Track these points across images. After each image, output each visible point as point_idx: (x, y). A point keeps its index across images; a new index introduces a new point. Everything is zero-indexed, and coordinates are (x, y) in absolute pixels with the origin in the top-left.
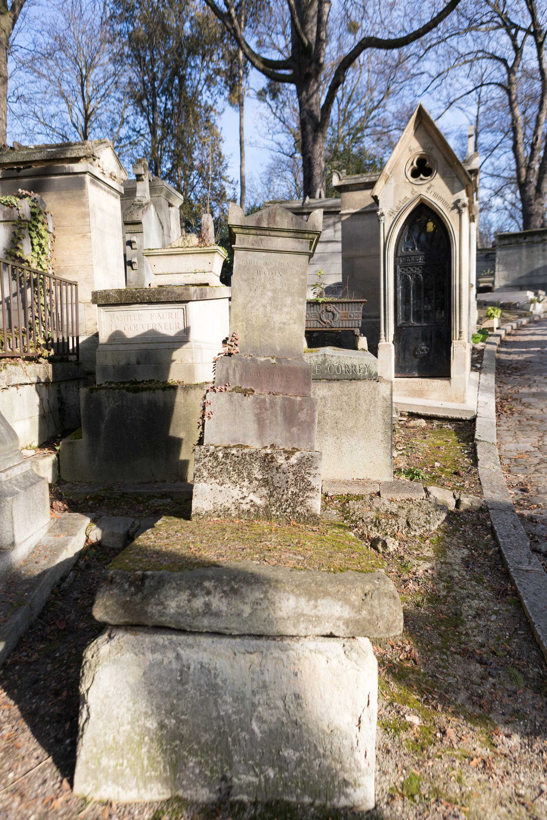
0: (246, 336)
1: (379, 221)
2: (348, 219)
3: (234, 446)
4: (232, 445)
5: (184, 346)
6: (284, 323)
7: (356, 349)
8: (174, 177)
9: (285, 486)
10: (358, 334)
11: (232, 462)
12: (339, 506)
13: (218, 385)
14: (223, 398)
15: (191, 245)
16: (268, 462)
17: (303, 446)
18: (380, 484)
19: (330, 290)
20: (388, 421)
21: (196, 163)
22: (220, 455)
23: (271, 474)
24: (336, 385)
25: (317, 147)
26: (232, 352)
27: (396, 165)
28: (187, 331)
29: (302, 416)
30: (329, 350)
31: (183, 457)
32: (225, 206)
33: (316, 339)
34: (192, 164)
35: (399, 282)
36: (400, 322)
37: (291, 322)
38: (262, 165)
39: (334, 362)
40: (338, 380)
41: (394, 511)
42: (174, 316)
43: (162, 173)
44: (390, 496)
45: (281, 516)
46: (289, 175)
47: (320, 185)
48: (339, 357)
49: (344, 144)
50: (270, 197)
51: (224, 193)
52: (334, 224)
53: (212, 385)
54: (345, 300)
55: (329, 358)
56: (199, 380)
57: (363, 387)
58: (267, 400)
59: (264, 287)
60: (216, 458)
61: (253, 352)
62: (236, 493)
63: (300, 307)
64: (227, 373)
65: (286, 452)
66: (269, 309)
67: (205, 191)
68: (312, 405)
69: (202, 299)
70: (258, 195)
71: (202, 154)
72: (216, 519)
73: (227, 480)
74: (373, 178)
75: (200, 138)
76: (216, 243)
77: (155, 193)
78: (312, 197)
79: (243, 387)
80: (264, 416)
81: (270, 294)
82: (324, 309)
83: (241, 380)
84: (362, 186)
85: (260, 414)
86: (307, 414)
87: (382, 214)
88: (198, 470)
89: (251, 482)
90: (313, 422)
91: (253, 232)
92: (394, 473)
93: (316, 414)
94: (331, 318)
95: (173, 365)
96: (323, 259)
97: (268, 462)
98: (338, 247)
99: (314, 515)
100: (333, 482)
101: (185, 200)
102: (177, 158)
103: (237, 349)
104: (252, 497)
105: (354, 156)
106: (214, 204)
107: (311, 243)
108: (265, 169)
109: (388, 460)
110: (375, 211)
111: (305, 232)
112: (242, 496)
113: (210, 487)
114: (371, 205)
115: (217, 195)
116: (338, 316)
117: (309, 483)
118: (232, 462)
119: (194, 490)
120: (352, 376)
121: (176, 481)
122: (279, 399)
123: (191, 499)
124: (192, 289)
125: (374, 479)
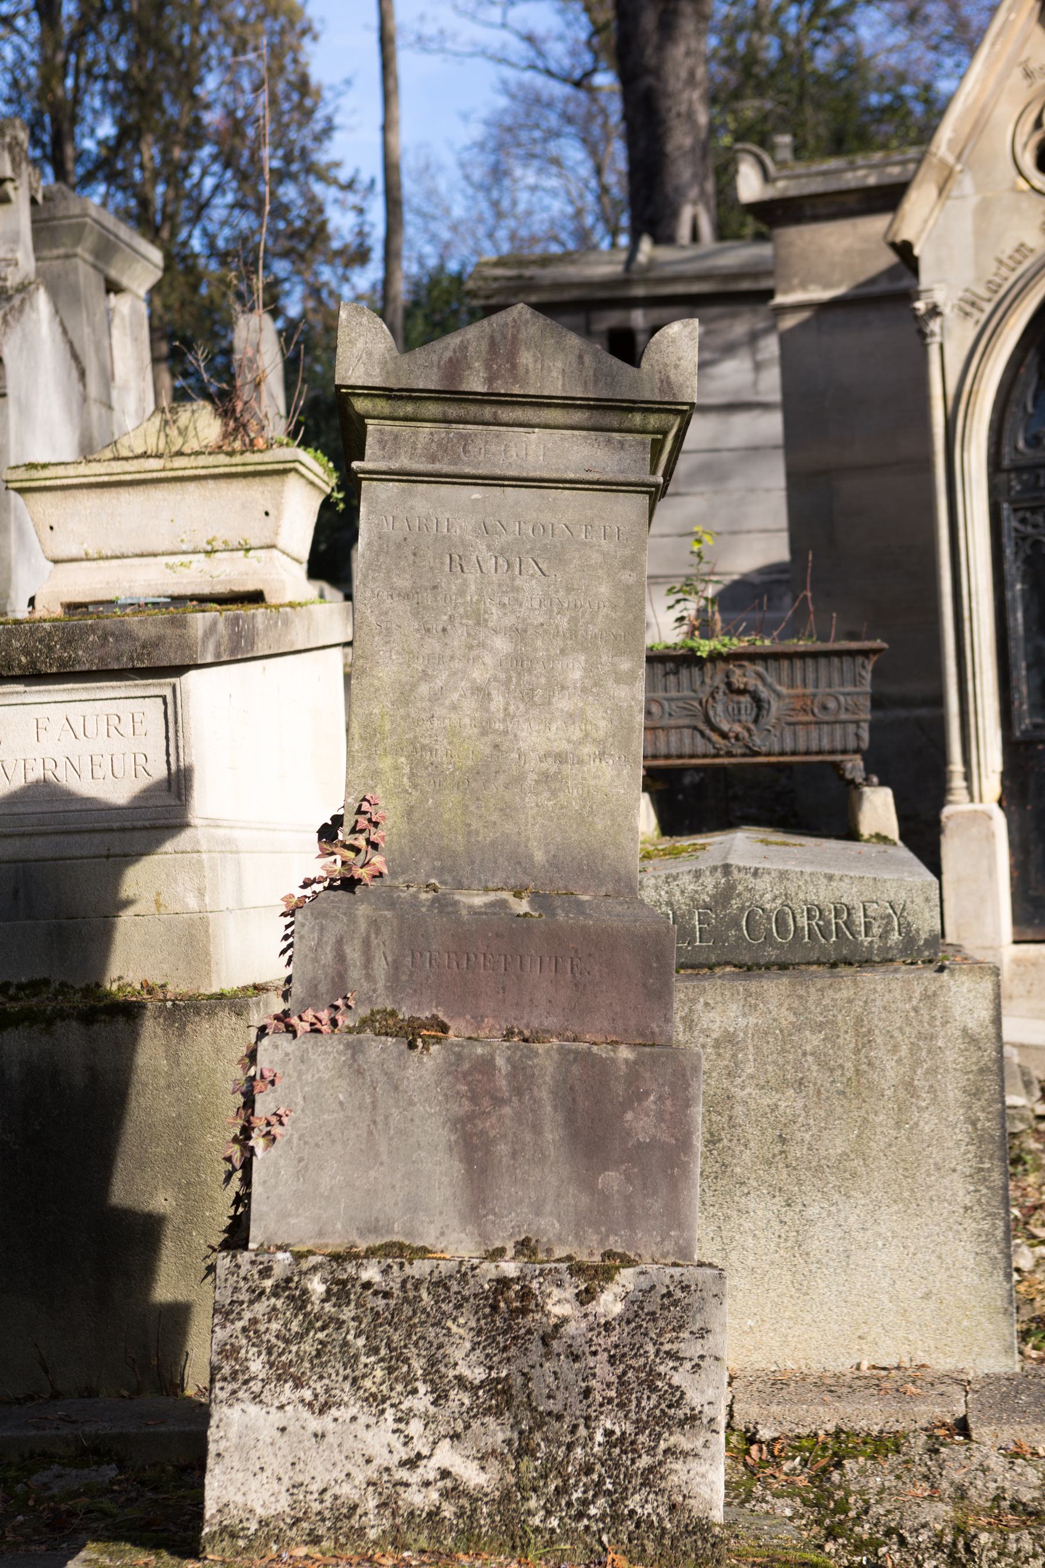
0: (410, 812)
1: (923, 335)
2: (803, 325)
3: (371, 1253)
4: (362, 1246)
5: (169, 846)
6: (560, 758)
7: (851, 834)
8: (124, 173)
9: (578, 1408)
10: (859, 777)
11: (365, 1318)
12: (802, 1481)
13: (304, 1006)
14: (325, 1057)
15: (193, 445)
16: (507, 1312)
17: (647, 1244)
18: (965, 1385)
19: (743, 597)
20: (989, 1124)
21: (212, 118)
22: (317, 1286)
23: (523, 1363)
24: (774, 989)
25: (678, 51)
26: (359, 873)
27: (979, 126)
28: (177, 784)
29: (642, 1124)
30: (743, 846)
31: (167, 1288)
32: (327, 274)
33: (689, 799)
34: (197, 121)
35: (1012, 568)
36: (1024, 724)
37: (588, 749)
38: (465, 117)
39: (766, 893)
40: (783, 967)
41: (1026, 1496)
42: (126, 728)
43: (80, 156)
44: (1008, 1434)
45: (568, 1533)
46: (574, 153)
47: (693, 193)
48: (783, 875)
49: (782, 34)
50: (502, 234)
51: (322, 227)
52: (753, 338)
53: (278, 1006)
54: (802, 645)
55: (743, 882)
56: (230, 974)
57: (885, 992)
58: (500, 1061)
59: (480, 620)
60: (300, 1301)
61: (440, 872)
62: (381, 1441)
63: (622, 692)
64: (340, 957)
65: (578, 1270)
66: (498, 702)
67: (245, 222)
68: (678, 1074)
69: (239, 651)
70: (454, 228)
71: (234, 85)
72: (301, 1551)
73: (344, 1392)
74: (895, 170)
75: (227, 25)
76: (293, 435)
77: (54, 244)
78: (664, 237)
79: (405, 1013)
80: (489, 1125)
81: (501, 644)
82: (719, 680)
83: (394, 985)
84: (851, 201)
85: (470, 1118)
86: (660, 1117)
87: (934, 311)
88: (228, 1351)
89: (440, 1398)
90: (685, 1144)
91: (433, 409)
92: (1024, 1336)
93: (698, 1111)
94: (747, 718)
95: (125, 920)
96: (715, 471)
97: (507, 1312)
98: (771, 426)
99: (701, 1528)
100: (777, 1384)
101: (168, 257)
102: (138, 103)
103: (378, 860)
104: (446, 1456)
105: (822, 80)
106: (281, 267)
107: (657, 447)
108: (476, 131)
109: (996, 1288)
110: (910, 295)
111: (630, 406)
112: (404, 1454)
113: (277, 1418)
114: (890, 273)
115: (295, 234)
116: (775, 707)
117: (676, 1397)
118: (365, 1318)
119: (212, 1434)
120: (834, 950)
121: (137, 1392)
122: (546, 1055)
123: (202, 1468)
124: (200, 621)
125: (942, 1363)
